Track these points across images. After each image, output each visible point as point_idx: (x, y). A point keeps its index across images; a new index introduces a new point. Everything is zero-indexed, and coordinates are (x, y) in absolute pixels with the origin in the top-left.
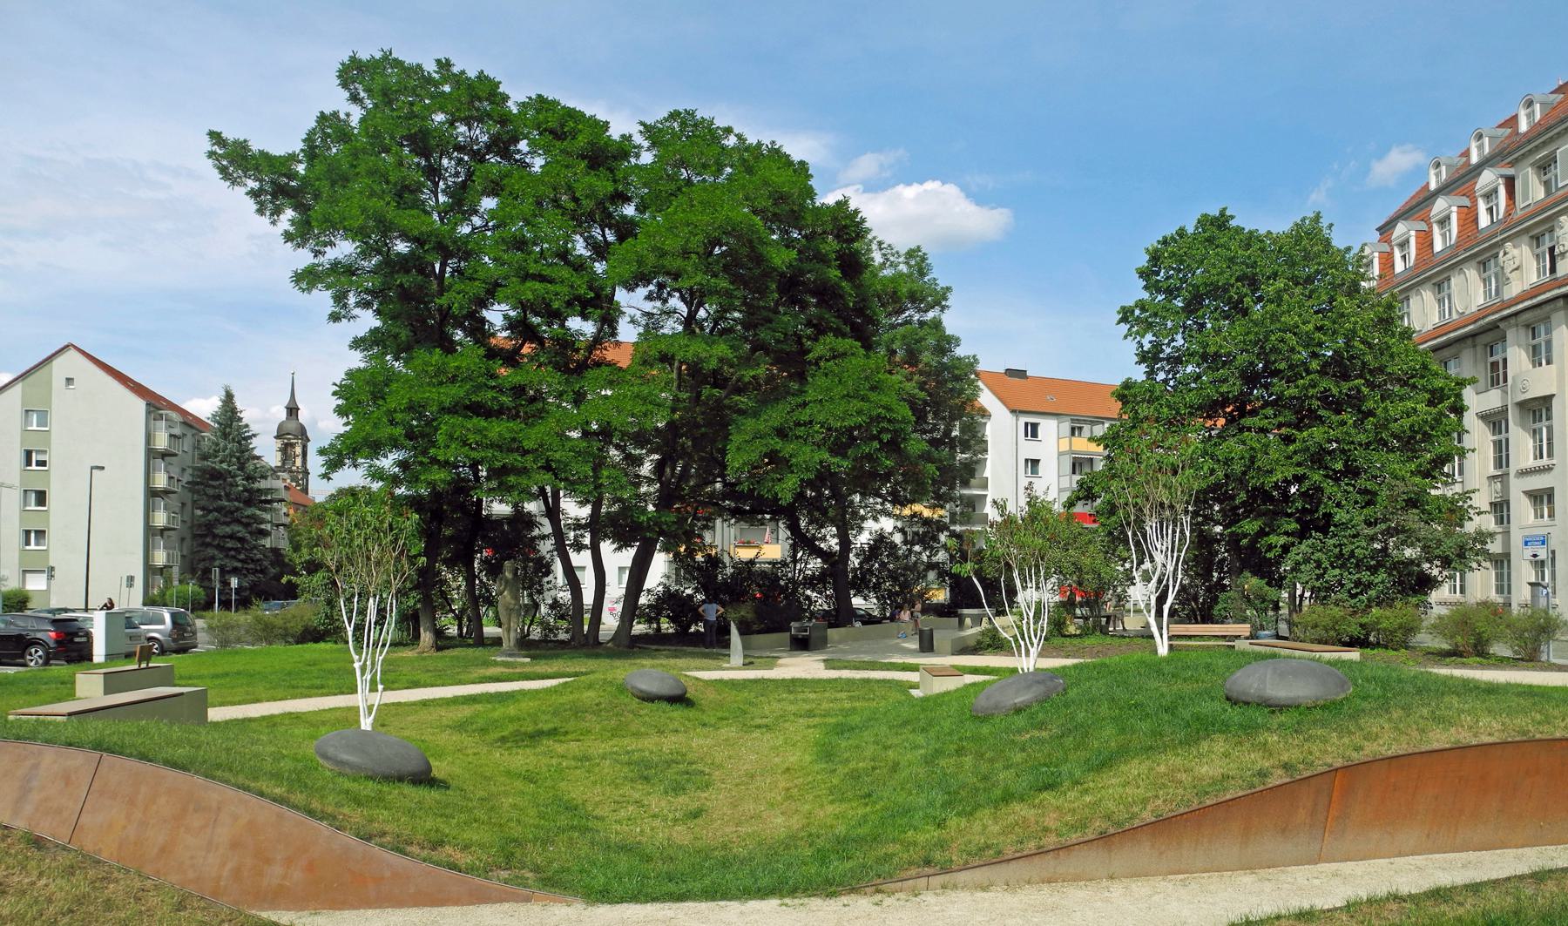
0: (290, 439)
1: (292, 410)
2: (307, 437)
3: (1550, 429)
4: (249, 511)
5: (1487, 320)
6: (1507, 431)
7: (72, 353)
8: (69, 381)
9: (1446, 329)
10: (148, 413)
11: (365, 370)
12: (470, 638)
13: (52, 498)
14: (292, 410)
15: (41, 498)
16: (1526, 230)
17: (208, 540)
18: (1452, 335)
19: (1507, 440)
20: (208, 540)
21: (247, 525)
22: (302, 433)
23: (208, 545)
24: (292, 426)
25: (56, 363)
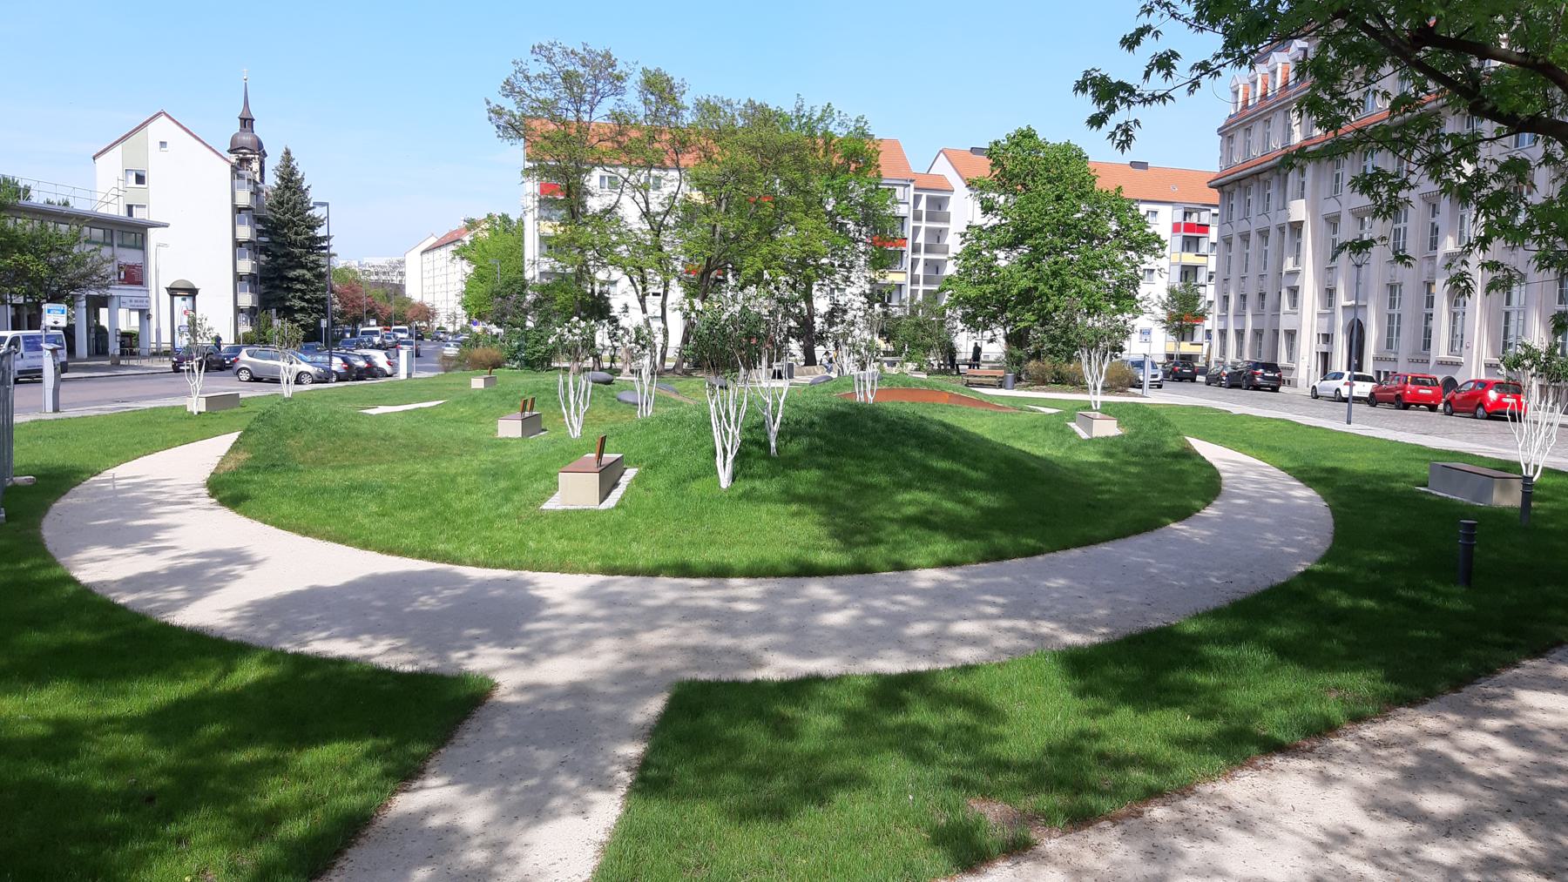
0: (245, 154)
1: (247, 122)
2: (264, 152)
3: (637, 293)
4: (312, 258)
5: (132, 405)
6: (1406, 221)
7: (163, 118)
8: (163, 144)
9: (1232, 170)
10: (233, 172)
11: (998, 510)
12: (589, 344)
13: (150, 178)
14: (247, 122)
15: (140, 179)
16: (1262, 116)
17: (277, 282)
18: (1236, 175)
19: (1405, 229)
20: (277, 282)
21: (310, 270)
22: (259, 149)
23: (278, 287)
24: (246, 139)
25: (150, 126)
